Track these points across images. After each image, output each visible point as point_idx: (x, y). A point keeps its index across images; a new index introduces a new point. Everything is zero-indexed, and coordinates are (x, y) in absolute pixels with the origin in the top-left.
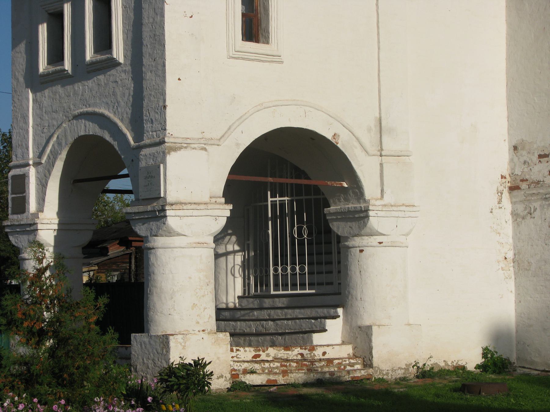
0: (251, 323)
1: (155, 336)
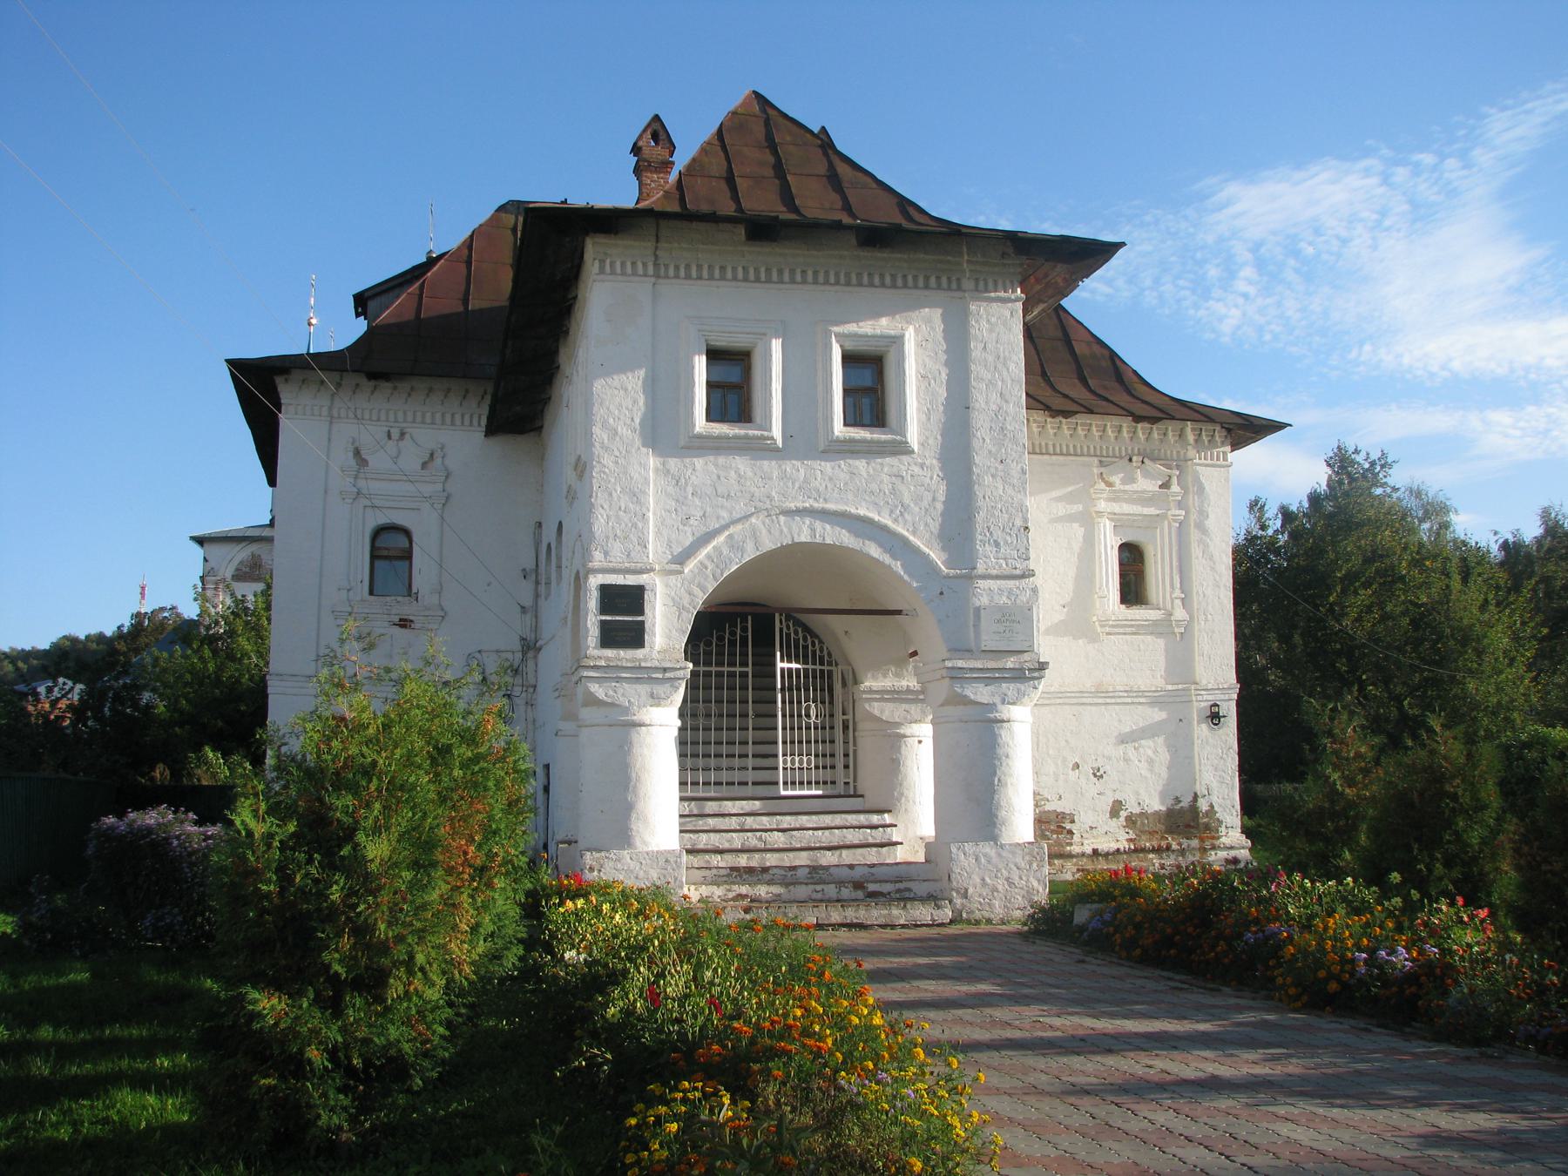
0: (734, 835)
1: (1010, 845)
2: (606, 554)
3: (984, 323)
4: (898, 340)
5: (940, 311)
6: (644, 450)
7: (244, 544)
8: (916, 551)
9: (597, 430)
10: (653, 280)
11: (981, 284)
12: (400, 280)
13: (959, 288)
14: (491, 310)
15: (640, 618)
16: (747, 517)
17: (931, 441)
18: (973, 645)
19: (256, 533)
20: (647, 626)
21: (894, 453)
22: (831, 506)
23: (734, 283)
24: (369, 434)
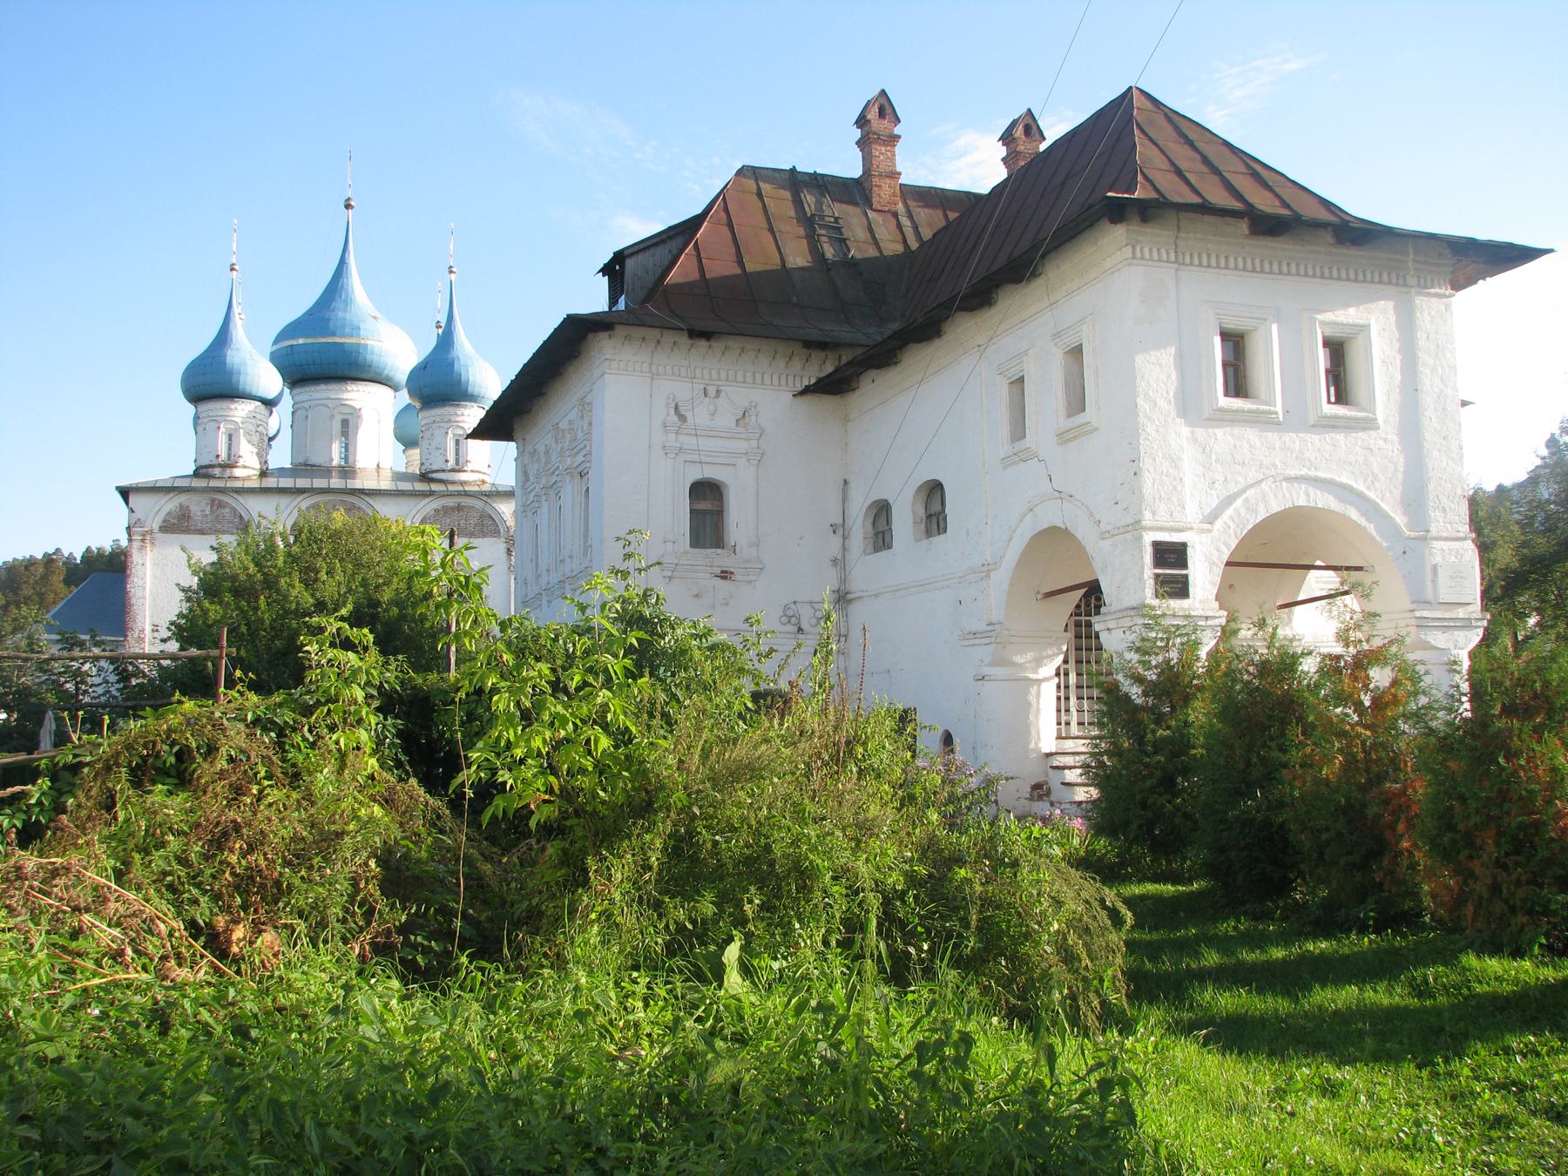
2: (1154, 513)
3: (1426, 315)
4: (1364, 329)
5: (1391, 304)
6: (1178, 420)
7: (172, 495)
9: (1140, 401)
10: (1176, 266)
11: (1422, 281)
12: (655, 241)
13: (1405, 285)
14: (766, 271)
15: (1184, 572)
16: (1259, 482)
18: (1430, 597)
19: (185, 483)
20: (1190, 578)
21: (1364, 429)
22: (1321, 474)
23: (1271, 276)
24: (683, 390)
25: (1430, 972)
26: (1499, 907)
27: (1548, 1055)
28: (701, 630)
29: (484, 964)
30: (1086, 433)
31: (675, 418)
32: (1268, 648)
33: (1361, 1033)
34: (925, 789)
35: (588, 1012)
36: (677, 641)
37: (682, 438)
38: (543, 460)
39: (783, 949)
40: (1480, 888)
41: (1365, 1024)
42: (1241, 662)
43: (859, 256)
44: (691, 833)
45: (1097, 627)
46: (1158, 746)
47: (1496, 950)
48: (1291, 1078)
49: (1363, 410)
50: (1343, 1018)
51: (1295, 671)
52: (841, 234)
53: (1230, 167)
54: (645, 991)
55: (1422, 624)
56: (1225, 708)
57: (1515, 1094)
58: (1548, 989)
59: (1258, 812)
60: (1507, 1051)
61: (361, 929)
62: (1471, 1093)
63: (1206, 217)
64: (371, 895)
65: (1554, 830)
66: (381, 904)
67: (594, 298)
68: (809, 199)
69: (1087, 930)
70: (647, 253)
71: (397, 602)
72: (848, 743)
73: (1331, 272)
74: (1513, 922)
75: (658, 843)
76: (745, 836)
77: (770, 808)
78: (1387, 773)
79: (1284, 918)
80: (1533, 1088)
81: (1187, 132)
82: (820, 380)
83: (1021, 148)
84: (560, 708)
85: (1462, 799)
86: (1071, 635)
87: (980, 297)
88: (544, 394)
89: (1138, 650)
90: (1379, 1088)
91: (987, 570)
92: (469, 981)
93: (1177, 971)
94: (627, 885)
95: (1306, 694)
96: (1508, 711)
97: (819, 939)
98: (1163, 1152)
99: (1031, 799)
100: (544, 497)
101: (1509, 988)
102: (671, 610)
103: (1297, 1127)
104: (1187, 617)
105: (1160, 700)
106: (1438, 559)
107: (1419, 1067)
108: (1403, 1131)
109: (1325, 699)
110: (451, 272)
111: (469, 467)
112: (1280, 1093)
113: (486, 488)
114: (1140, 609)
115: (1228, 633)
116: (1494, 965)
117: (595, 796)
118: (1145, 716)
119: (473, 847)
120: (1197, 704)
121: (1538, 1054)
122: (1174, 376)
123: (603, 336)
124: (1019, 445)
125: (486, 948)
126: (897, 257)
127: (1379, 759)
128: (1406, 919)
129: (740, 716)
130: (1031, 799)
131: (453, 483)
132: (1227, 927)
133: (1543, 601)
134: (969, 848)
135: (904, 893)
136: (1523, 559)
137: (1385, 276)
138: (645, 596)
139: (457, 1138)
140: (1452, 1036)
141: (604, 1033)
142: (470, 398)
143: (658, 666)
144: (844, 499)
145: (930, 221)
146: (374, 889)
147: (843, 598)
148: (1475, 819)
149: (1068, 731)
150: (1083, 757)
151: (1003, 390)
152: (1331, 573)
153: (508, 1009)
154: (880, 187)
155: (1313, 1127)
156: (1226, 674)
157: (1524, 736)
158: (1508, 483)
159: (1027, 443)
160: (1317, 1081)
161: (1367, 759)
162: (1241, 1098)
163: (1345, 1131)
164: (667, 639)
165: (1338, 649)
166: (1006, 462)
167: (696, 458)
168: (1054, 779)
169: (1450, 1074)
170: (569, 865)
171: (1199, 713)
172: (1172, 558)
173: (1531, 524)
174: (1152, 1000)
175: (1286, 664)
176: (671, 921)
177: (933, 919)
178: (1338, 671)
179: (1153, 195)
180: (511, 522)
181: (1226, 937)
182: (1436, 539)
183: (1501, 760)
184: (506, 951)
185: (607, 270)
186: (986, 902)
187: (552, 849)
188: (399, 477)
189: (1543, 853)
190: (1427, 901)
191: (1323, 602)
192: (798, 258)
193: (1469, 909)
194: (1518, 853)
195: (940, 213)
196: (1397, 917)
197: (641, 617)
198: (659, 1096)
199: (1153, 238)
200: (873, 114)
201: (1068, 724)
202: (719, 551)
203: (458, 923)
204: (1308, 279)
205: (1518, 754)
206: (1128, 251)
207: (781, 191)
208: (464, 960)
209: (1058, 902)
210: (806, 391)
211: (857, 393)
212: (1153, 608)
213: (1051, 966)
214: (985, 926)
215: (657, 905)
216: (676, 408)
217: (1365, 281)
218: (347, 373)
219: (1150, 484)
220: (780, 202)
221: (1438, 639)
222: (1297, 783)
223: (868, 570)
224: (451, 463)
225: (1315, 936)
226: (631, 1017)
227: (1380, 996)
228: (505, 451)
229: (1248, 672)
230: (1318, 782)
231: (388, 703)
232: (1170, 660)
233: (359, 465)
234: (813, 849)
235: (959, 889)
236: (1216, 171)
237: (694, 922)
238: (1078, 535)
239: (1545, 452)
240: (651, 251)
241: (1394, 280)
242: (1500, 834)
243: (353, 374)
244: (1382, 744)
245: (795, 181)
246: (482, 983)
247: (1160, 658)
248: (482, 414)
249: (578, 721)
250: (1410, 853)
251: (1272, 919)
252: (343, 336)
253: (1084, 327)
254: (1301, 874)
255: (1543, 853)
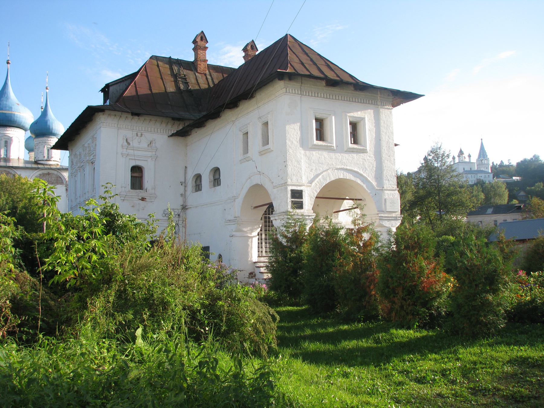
2: (291, 180)
3: (384, 115)
4: (363, 119)
5: (372, 111)
6: (300, 148)
8: (369, 182)
9: (287, 141)
12: (120, 81)
13: (377, 105)
14: (160, 93)
15: (301, 200)
17: (372, 149)
18: (384, 210)
21: (363, 153)
22: (348, 168)
24: (129, 134)
25: (380, 335)
26: (403, 313)
27: (417, 361)
28: (131, 219)
29: (49, 337)
30: (269, 152)
31: (126, 144)
32: (329, 226)
33: (357, 356)
34: (210, 274)
35: (85, 353)
36: (123, 222)
37: (128, 151)
38: (79, 157)
39: (157, 330)
40: (397, 307)
41: (358, 353)
42: (319, 231)
43: (192, 89)
44: (125, 290)
45: (272, 219)
46: (291, 260)
47: (402, 327)
48: (333, 372)
49: (362, 146)
50: (351, 351)
51: (338, 234)
52: (186, 81)
53: (320, 63)
54: (108, 346)
55: (381, 219)
56: (314, 246)
57: (405, 374)
58: (418, 339)
59: (325, 282)
60: (404, 360)
61: (3, 326)
62: (392, 375)
63: (311, 79)
64: (7, 313)
65: (421, 287)
66: (11, 317)
67: (98, 100)
68: (175, 68)
69: (264, 323)
70: (117, 85)
71: (24, 207)
72: (182, 258)
73: (352, 99)
74: (407, 318)
75: (113, 293)
76: (144, 291)
77: (154, 280)
78: (368, 268)
79: (333, 318)
80: (411, 372)
81: (305, 50)
82: (177, 132)
83: (250, 53)
84: (79, 246)
85: (392, 277)
86: (263, 221)
87: (233, 104)
88: (79, 134)
89: (285, 226)
90: (362, 374)
91: (234, 198)
92: (42, 344)
93: (297, 336)
94: (101, 309)
95: (341, 242)
96: (406, 248)
97: (170, 327)
98: (286, 398)
99: (249, 278)
100: (79, 171)
101: (405, 340)
102: (121, 211)
103: (333, 388)
104: (302, 215)
105: (292, 244)
106: (386, 197)
107: (375, 367)
108: (369, 388)
109: (348, 244)
110: (47, 89)
111: (53, 159)
112: (329, 377)
113: (58, 167)
114: (287, 213)
115: (316, 221)
116: (401, 332)
117: (91, 277)
118: (287, 250)
119: (47, 295)
120: (305, 245)
121: (413, 361)
122: (299, 133)
123: (101, 114)
124: (246, 156)
125: (49, 332)
126: (205, 90)
127: (365, 264)
128: (375, 318)
129: (146, 249)
130: (249, 278)
131: (47, 165)
132: (314, 321)
133: (421, 211)
134: (223, 295)
135: (200, 310)
136: (415, 197)
137: (370, 102)
138: (112, 206)
139: (33, 401)
140: (386, 356)
141: (92, 361)
142: (54, 135)
143: (117, 231)
144: (185, 173)
145: (217, 77)
146: (8, 311)
147: (184, 208)
148: (396, 284)
149: (262, 254)
150: (266, 263)
151: (241, 136)
152: (351, 201)
153: (57, 353)
154: (200, 65)
155: (339, 388)
156: (314, 235)
157: (411, 256)
158: (411, 171)
159: (249, 155)
160: (342, 372)
161: (361, 264)
162: (316, 379)
163: (350, 389)
164: (119, 222)
165: (352, 227)
166: (241, 161)
167: (133, 158)
168: (257, 271)
169: (385, 369)
170: (81, 302)
171: (306, 248)
172: (297, 195)
173: (418, 186)
174: (288, 346)
175: (335, 231)
176: (117, 321)
177: (210, 319)
178: (352, 234)
179: (294, 71)
180: (67, 179)
181: (314, 325)
182: (386, 190)
183: (404, 264)
184: (57, 333)
185: (103, 90)
186: (229, 313)
187: (76, 295)
188: (26, 162)
189: (417, 295)
190: (380, 312)
191: (348, 211)
192: (171, 88)
193: (393, 314)
194: (409, 295)
195: (221, 74)
196: (370, 317)
197: (110, 214)
198: (110, 383)
199: (293, 86)
200: (198, 40)
201: (262, 252)
202: (141, 191)
203: (40, 323)
204: (345, 102)
205: (410, 262)
206: (284, 90)
207: (166, 65)
208: (41, 336)
209: (254, 313)
210: (173, 135)
211: (191, 136)
212: (290, 212)
213: (251, 335)
214: (229, 320)
215: (113, 315)
216: (127, 140)
217: (364, 103)
218: (7, 124)
219: (290, 169)
220: (166, 69)
221: (387, 224)
222: (338, 272)
223: (193, 198)
224: (46, 158)
225: (344, 324)
226: (102, 355)
227: (364, 343)
228: (65, 154)
229: (322, 234)
230: (345, 272)
231: (17, 244)
232: (296, 230)
233: (11, 158)
234: (168, 294)
235: (220, 309)
236: (315, 64)
237: (126, 322)
238: (266, 187)
239: (423, 162)
240: (119, 84)
241: (373, 103)
242: (403, 289)
243: (9, 125)
244: (366, 259)
245: (170, 62)
246: (48, 344)
247: (293, 229)
248: (57, 140)
249: (85, 251)
250: (375, 295)
251: (330, 318)
252: (6, 110)
253: (269, 116)
254: (339, 303)
255: (417, 295)
